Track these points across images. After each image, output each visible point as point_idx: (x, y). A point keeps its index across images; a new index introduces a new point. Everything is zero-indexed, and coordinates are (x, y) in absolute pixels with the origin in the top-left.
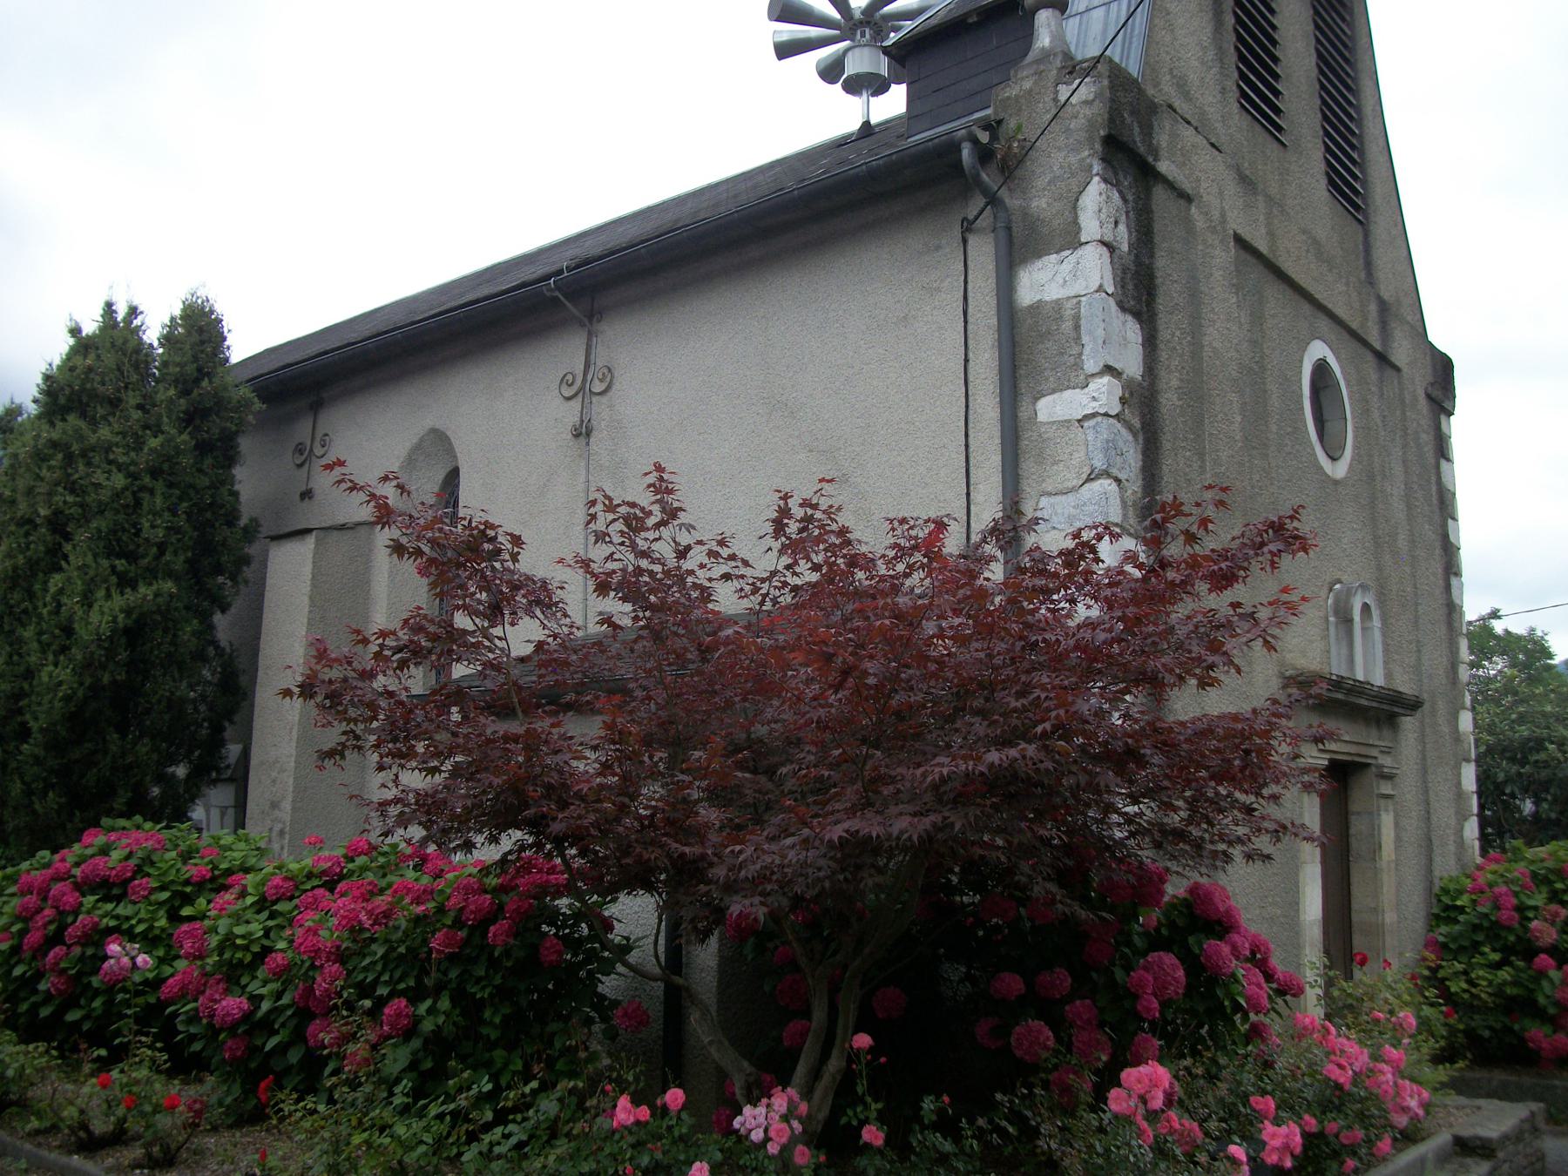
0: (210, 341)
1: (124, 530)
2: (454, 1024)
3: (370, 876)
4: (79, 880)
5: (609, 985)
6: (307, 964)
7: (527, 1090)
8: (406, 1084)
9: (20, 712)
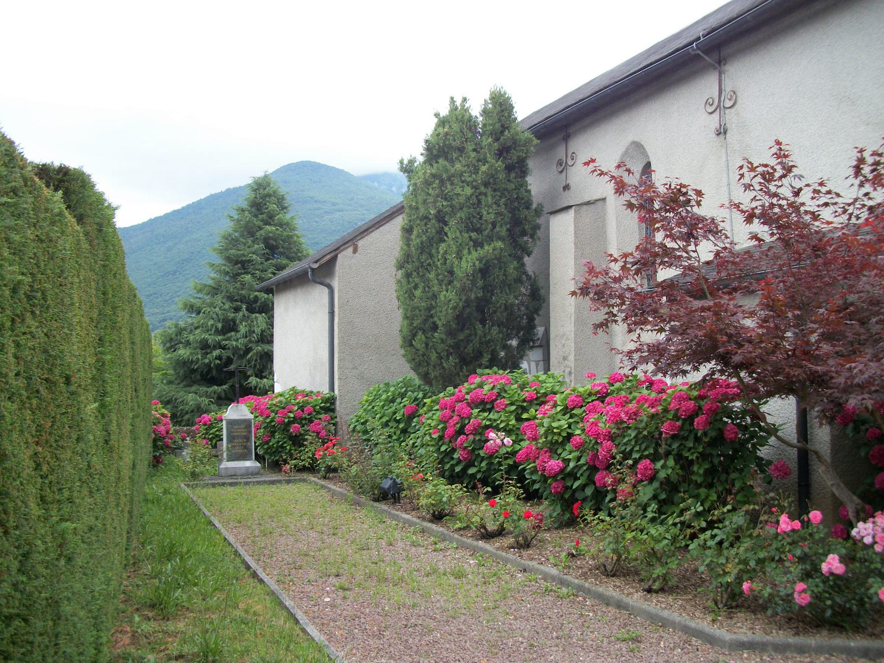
0: (506, 110)
1: (474, 217)
2: (677, 474)
3: (623, 393)
4: (469, 401)
5: (763, 452)
6: (593, 442)
7: (725, 510)
8: (654, 506)
9: (432, 316)
